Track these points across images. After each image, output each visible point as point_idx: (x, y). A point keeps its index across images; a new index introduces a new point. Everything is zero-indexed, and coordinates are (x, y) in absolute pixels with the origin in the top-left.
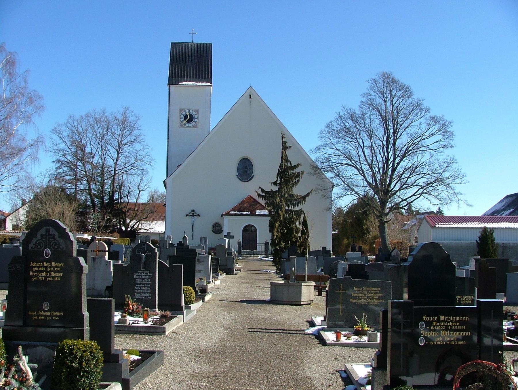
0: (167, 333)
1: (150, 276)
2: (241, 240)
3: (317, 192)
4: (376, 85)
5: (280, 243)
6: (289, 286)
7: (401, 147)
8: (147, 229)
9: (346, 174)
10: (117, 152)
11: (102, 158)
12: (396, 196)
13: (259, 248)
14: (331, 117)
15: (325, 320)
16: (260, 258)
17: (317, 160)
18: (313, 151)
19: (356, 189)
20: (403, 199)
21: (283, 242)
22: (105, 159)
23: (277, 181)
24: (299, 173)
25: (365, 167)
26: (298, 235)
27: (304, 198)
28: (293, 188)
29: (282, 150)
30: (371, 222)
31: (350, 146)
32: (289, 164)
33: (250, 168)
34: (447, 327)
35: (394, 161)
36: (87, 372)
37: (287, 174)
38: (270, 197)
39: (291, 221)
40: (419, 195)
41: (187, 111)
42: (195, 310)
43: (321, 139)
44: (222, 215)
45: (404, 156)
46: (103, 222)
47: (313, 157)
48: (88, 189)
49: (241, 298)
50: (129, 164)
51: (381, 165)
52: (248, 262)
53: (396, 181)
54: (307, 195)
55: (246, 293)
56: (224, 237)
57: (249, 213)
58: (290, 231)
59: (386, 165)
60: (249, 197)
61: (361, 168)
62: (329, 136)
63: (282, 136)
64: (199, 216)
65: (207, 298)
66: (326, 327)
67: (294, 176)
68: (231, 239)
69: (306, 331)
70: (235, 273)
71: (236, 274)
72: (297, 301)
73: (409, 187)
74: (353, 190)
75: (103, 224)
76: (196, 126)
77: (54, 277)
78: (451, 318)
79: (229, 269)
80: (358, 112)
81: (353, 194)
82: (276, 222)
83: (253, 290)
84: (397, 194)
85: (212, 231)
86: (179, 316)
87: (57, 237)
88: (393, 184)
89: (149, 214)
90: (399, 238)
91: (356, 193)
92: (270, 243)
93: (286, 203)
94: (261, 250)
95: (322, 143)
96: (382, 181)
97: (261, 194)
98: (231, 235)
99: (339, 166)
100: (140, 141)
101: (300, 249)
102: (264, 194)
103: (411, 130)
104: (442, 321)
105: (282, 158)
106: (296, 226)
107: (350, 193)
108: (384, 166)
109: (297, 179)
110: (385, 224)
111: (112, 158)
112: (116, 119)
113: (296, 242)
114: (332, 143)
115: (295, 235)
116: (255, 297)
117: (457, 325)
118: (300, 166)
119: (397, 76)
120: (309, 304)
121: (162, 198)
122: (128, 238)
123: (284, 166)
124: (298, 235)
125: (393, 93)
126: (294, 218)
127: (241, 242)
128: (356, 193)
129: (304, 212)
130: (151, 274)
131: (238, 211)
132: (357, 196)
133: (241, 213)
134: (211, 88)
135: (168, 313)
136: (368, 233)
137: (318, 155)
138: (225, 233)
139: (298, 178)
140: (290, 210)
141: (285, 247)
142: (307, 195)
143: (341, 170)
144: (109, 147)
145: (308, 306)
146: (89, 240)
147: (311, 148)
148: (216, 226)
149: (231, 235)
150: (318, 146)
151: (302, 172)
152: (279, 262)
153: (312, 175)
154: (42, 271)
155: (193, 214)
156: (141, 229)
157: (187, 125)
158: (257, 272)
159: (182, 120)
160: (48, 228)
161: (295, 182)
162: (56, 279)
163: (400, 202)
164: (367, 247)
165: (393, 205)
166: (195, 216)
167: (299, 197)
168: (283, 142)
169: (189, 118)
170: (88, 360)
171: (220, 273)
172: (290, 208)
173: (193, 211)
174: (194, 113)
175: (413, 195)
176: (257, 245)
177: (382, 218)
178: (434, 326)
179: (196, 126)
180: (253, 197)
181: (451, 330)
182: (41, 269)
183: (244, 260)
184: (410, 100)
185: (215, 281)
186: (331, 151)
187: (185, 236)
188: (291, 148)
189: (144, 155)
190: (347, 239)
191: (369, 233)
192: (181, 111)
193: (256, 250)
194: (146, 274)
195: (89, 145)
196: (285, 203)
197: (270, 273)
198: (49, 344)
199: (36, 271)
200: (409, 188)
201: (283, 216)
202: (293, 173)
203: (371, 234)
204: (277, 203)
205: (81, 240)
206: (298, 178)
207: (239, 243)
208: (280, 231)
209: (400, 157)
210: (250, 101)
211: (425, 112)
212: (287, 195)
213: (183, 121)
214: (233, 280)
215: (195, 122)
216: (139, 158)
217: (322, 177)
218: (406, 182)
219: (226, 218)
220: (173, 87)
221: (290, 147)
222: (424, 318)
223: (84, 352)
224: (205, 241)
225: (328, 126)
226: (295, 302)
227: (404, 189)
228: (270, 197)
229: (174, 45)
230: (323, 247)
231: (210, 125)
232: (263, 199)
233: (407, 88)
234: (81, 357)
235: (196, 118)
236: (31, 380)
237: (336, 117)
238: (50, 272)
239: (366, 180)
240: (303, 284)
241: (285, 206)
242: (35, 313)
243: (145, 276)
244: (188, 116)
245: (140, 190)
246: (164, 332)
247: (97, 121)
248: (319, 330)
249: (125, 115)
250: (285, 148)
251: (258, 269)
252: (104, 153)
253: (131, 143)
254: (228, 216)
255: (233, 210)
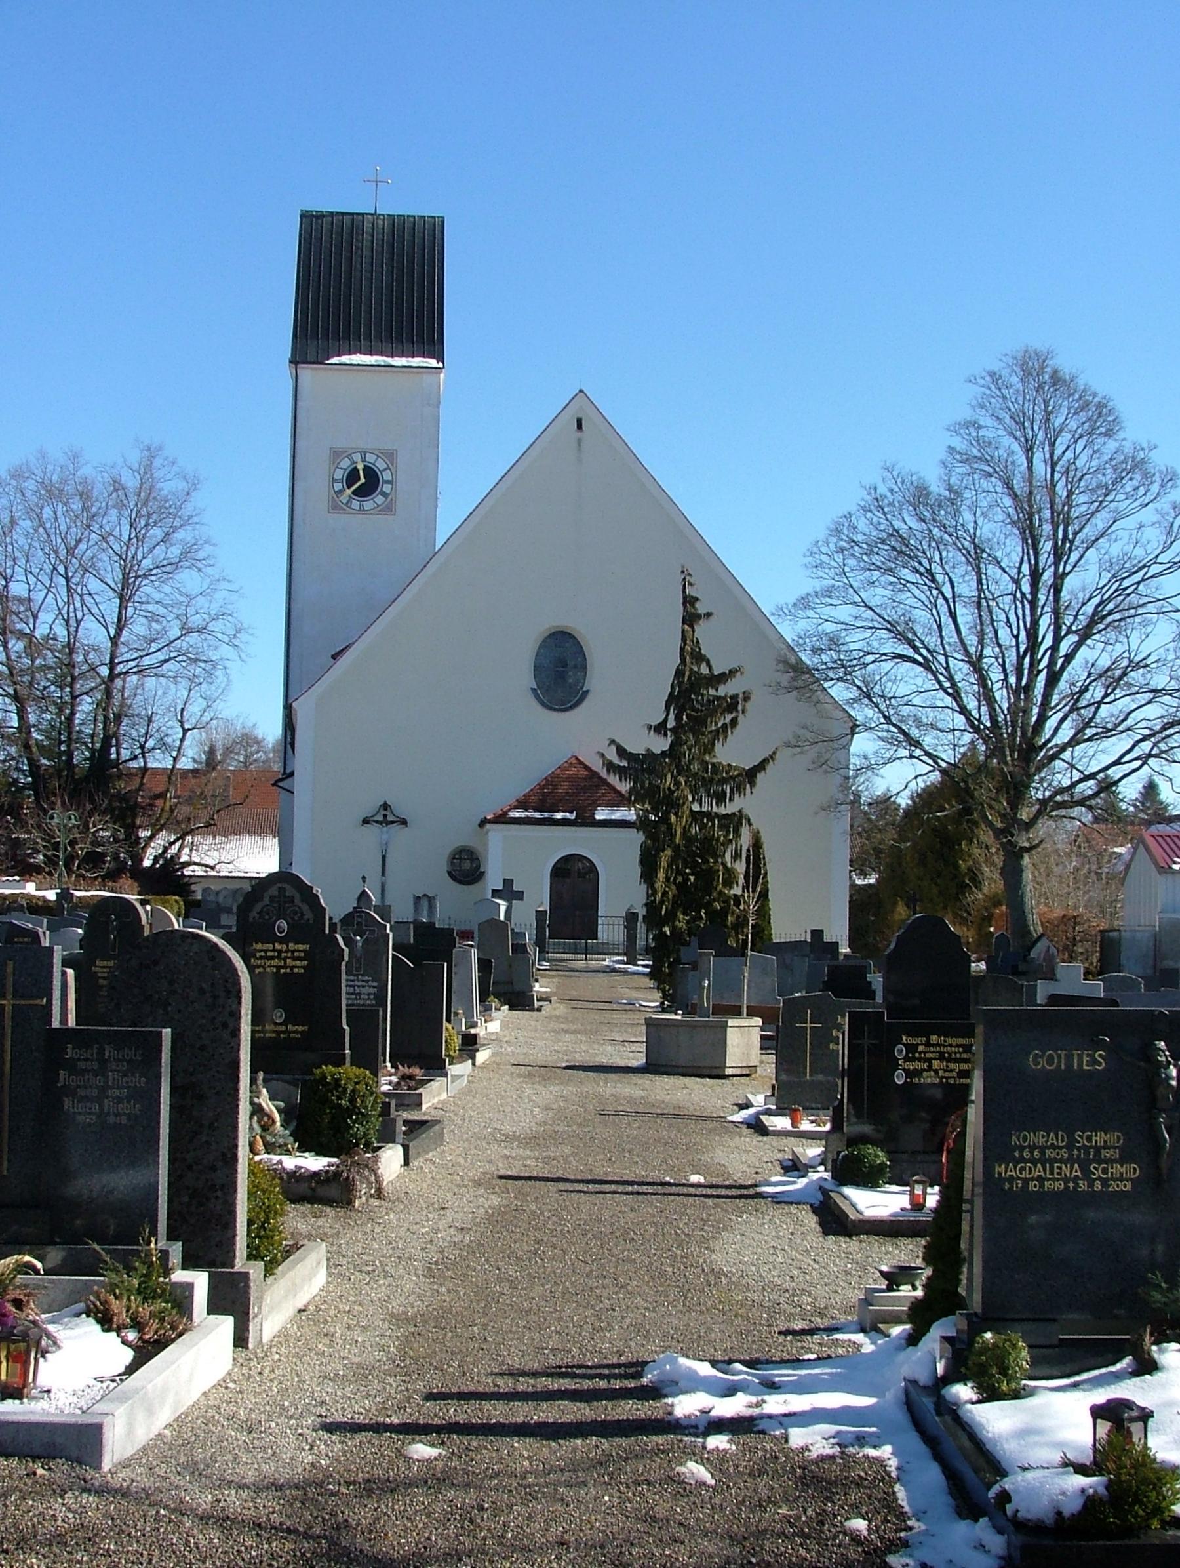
0: (424, 1107)
1: (374, 987)
2: (546, 907)
3: (798, 749)
4: (998, 393)
5: (675, 917)
6: (693, 1026)
7: (1081, 600)
8: (212, 863)
9: (893, 690)
10: (118, 601)
11: (67, 621)
12: (1058, 764)
13: (603, 933)
14: (851, 499)
15: (773, 1095)
16: (608, 966)
17: (801, 641)
18: (786, 611)
19: (928, 741)
20: (1086, 773)
21: (685, 914)
22: (78, 625)
23: (665, 720)
24: (734, 697)
25: (961, 670)
26: (732, 892)
27: (751, 775)
28: (718, 746)
29: (684, 623)
30: (987, 846)
31: (909, 594)
32: (704, 670)
33: (575, 667)
34: (942, 1054)
35: (1054, 648)
36: (362, 1114)
37: (697, 701)
38: (643, 770)
39: (710, 848)
40: (1139, 763)
41: (357, 457)
42: (463, 1076)
43: (814, 569)
44: (483, 823)
45: (1085, 635)
46: (83, 841)
47: (788, 631)
48: (16, 725)
49: (567, 1061)
50: (162, 642)
51: (1011, 657)
52: (571, 977)
53: (1060, 715)
54: (761, 766)
55: (576, 1052)
56: (493, 897)
57: (573, 816)
58: (707, 878)
59: (1027, 660)
60: (575, 761)
61: (947, 668)
62: (841, 561)
63: (684, 579)
64: (404, 822)
65: (482, 1056)
66: (774, 1107)
67: (719, 706)
68: (514, 902)
69: (730, 1118)
70: (536, 1006)
71: (539, 1010)
72: (716, 1068)
73: (1106, 732)
74: (917, 744)
75: (82, 849)
76: (389, 509)
77: (292, 968)
78: (949, 1040)
79: (518, 993)
80: (937, 488)
81: (917, 758)
82: (663, 851)
83: (596, 1046)
84: (1066, 755)
85: (449, 873)
86: (438, 1079)
87: (297, 901)
88: (1051, 724)
89: (218, 811)
90: (1079, 902)
91: (927, 754)
92: (644, 916)
93: (694, 791)
94: (611, 938)
95: (818, 585)
96: (1018, 711)
97: (616, 760)
98: (515, 889)
99: (873, 662)
100: (199, 565)
101: (737, 935)
102: (624, 763)
103: (1114, 548)
104: (933, 1045)
105: (682, 649)
106: (724, 864)
107: (906, 753)
108: (1021, 659)
109: (729, 717)
110: (1022, 857)
111: (102, 620)
112: (117, 485)
113: (724, 912)
114: (852, 587)
115: (721, 893)
116: (604, 1060)
117: (959, 1052)
118: (739, 673)
119: (1065, 363)
120: (747, 1075)
121: (246, 750)
122: (177, 898)
123: (687, 673)
124: (732, 892)
125: (1058, 422)
126: (719, 837)
127: (546, 911)
128: (927, 754)
129: (749, 820)
130: (375, 984)
131: (536, 810)
132: (931, 762)
133: (546, 815)
134: (442, 376)
135: (417, 1071)
136: (976, 887)
137: (802, 625)
138: (494, 881)
139: (734, 715)
140: (708, 815)
141: (689, 929)
142: (761, 766)
143: (877, 678)
144: (94, 584)
145: (743, 1080)
146: (50, 901)
147: (782, 602)
148: (460, 859)
149: (515, 889)
150: (803, 593)
151: (744, 693)
152: (670, 974)
153: (784, 691)
154: (272, 958)
155: (385, 816)
156: (188, 864)
157: (355, 504)
158: (601, 1005)
159: (338, 486)
160: (280, 885)
161: (725, 725)
162: (296, 970)
163: (1074, 785)
164: (970, 934)
165: (1047, 794)
166: (393, 822)
167: (736, 773)
168: (685, 598)
169: (363, 480)
170: (363, 1096)
171: (494, 1005)
172: (705, 809)
173: (385, 806)
174: (380, 465)
175: (1117, 762)
176: (600, 921)
177: (1012, 836)
178: (920, 1053)
179: (389, 509)
180: (587, 763)
181: (949, 1060)
182: (269, 954)
183: (557, 970)
184: (1112, 445)
185: (486, 1022)
186: (845, 613)
187: (364, 891)
188: (711, 618)
189: (213, 612)
190: (907, 905)
191: (978, 884)
192: (337, 454)
193: (596, 939)
194: (364, 984)
195: (20, 574)
196: (691, 792)
197: (644, 1009)
198: (288, 1077)
199: (261, 958)
200: (1107, 737)
201: (685, 831)
202: (718, 698)
203: (986, 890)
204: (664, 789)
205: (24, 903)
206: (734, 715)
207: (540, 915)
208: (675, 879)
209: (1075, 632)
210: (579, 441)
211: (1162, 486)
212: (695, 767)
213: (341, 491)
214: (532, 1023)
215: (385, 495)
216: (196, 621)
217: (814, 699)
218: (1091, 720)
219: (497, 833)
220: (308, 373)
221: (708, 615)
222: (904, 1038)
223: (357, 1083)
224: (431, 908)
225: (838, 531)
226: (711, 1068)
227: (1090, 739)
228: (643, 770)
229: (306, 216)
230: (813, 932)
231: (436, 506)
232: (621, 780)
233: (1100, 406)
234: (353, 1091)
235: (388, 482)
236: (278, 1124)
237: (863, 499)
238: (285, 959)
239: (963, 711)
240: (731, 1022)
241: (690, 798)
242: (260, 1028)
243: (363, 986)
244: (361, 473)
245: (187, 726)
246: (420, 1105)
247: (52, 492)
248: (758, 1114)
249: (146, 470)
250: (691, 619)
251: (606, 996)
252: (78, 605)
253: (169, 568)
254: (503, 826)
255: (522, 804)
